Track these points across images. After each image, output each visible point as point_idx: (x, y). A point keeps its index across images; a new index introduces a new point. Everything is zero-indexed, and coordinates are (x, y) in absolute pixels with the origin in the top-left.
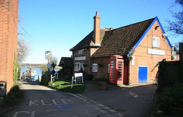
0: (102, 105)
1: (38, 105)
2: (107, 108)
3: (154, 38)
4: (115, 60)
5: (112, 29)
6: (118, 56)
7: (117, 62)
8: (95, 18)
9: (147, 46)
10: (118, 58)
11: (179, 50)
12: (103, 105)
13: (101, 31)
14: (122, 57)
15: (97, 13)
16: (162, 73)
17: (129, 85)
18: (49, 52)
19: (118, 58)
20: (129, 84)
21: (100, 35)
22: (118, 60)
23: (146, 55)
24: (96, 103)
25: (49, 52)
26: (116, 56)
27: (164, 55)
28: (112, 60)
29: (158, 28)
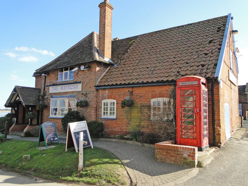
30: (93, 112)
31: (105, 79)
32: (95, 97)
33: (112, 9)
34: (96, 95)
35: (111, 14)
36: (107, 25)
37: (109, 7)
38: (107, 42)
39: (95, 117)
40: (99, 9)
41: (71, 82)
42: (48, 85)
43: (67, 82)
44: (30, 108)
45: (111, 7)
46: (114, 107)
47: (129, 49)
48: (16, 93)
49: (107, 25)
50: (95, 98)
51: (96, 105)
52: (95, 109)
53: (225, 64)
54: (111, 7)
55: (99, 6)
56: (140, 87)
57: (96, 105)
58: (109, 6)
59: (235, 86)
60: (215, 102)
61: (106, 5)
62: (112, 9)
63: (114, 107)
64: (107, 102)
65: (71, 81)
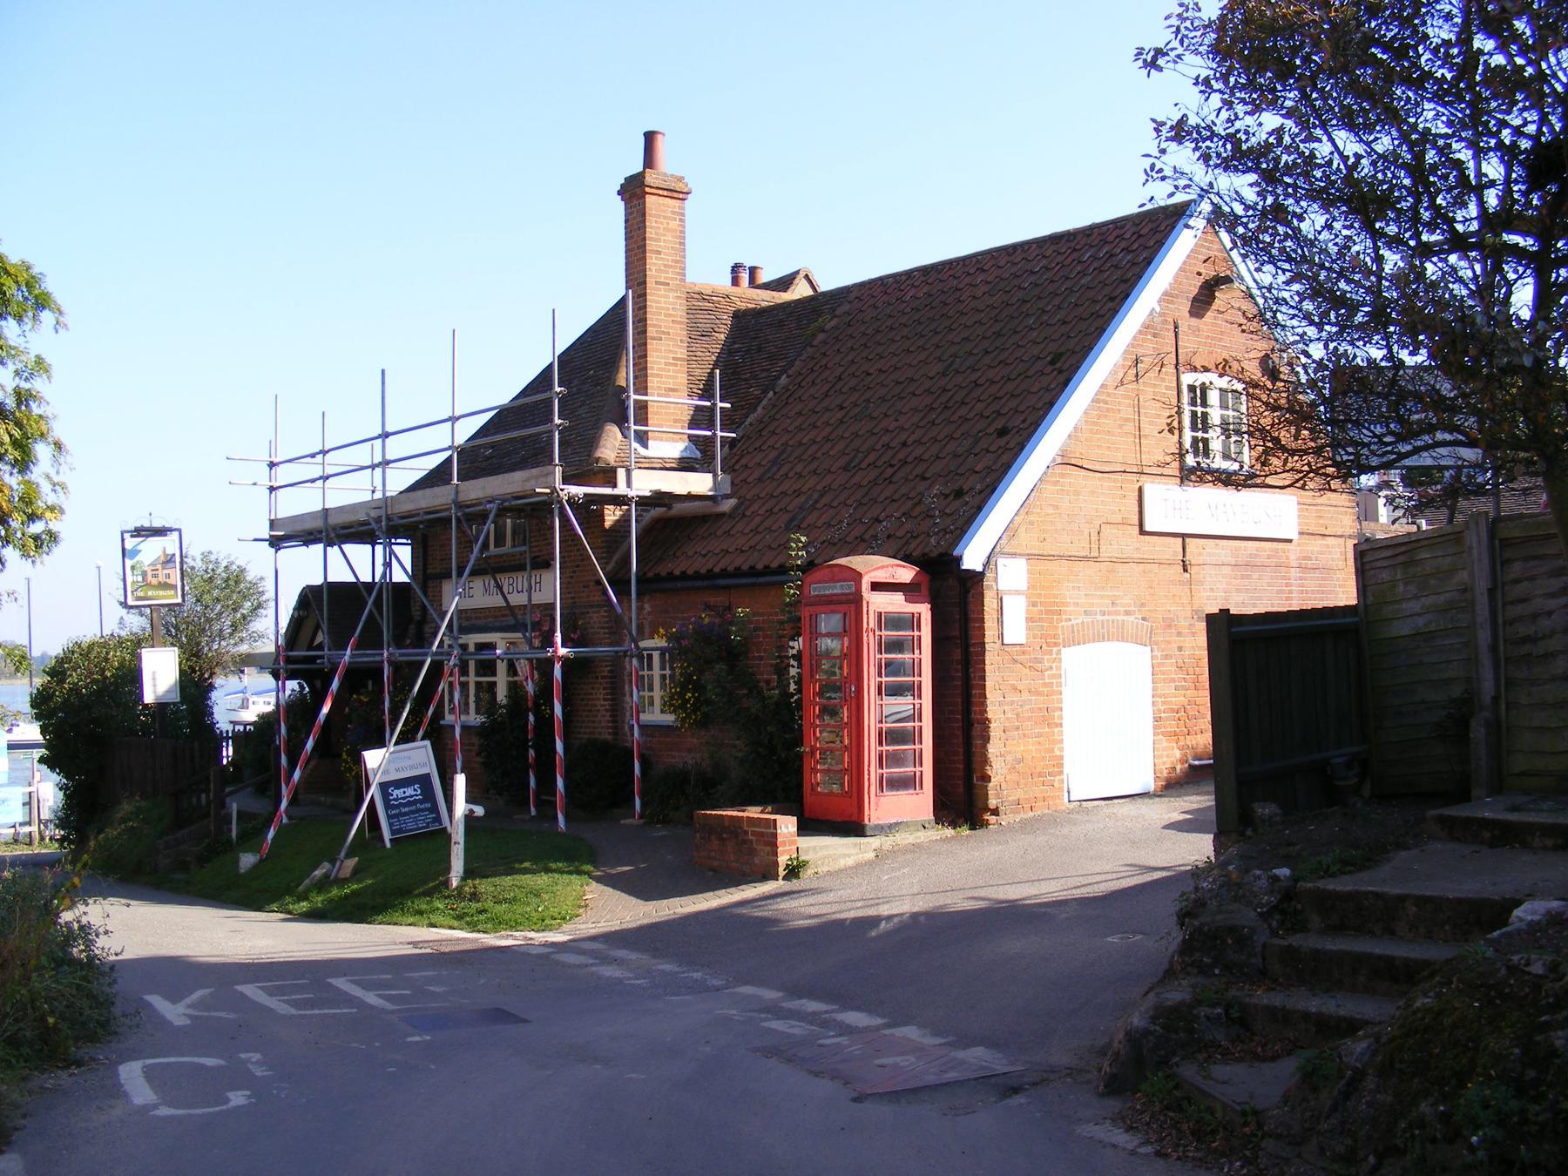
0: (770, 995)
1: (231, 1016)
2: (813, 1006)
3: (1192, 388)
4: (854, 602)
5: (801, 291)
6: (876, 567)
7: (869, 621)
8: (633, 191)
9: (1132, 459)
10: (876, 587)
11: (477, 817)
12: (778, 989)
13: (699, 303)
14: (906, 574)
15: (661, 145)
16: (32, 518)
17: (984, 824)
18: (161, 532)
19: (876, 587)
20: (987, 816)
21: (692, 358)
22: (879, 603)
23: (1129, 543)
24: (716, 982)
25: (161, 532)
26: (856, 562)
27: (1294, 535)
28: (830, 602)
29: (1222, 297)
30: (601, 697)
31: (988, 417)
32: (603, 631)
33: (681, 196)
34: (607, 622)
35: (681, 220)
36: (657, 283)
37: (665, 193)
38: (660, 363)
39: (609, 721)
40: (619, 206)
41: (518, 562)
42: (438, 571)
43: (505, 558)
44: (370, 683)
45: (676, 191)
46: (495, 683)
47: (785, 376)
48: (307, 617)
49: (657, 283)
50: (605, 633)
51: (609, 668)
52: (607, 683)
53: (1084, 472)
54: (676, 191)
55: (619, 193)
56: (737, 586)
57: (609, 668)
58: (661, 192)
59: (1290, 541)
60: (972, 649)
61: (647, 190)
62: (681, 196)
63: (495, 683)
64: (919, 611)
65: (518, 557)
